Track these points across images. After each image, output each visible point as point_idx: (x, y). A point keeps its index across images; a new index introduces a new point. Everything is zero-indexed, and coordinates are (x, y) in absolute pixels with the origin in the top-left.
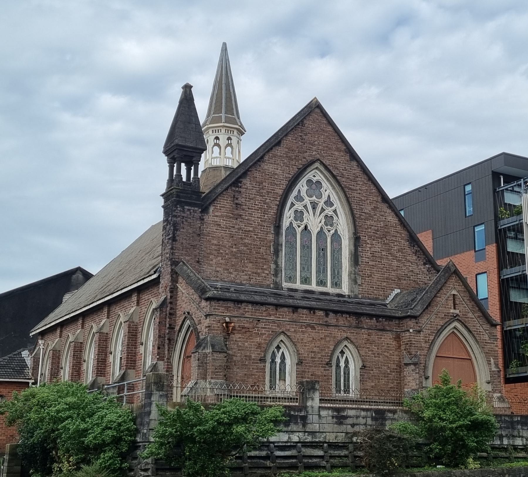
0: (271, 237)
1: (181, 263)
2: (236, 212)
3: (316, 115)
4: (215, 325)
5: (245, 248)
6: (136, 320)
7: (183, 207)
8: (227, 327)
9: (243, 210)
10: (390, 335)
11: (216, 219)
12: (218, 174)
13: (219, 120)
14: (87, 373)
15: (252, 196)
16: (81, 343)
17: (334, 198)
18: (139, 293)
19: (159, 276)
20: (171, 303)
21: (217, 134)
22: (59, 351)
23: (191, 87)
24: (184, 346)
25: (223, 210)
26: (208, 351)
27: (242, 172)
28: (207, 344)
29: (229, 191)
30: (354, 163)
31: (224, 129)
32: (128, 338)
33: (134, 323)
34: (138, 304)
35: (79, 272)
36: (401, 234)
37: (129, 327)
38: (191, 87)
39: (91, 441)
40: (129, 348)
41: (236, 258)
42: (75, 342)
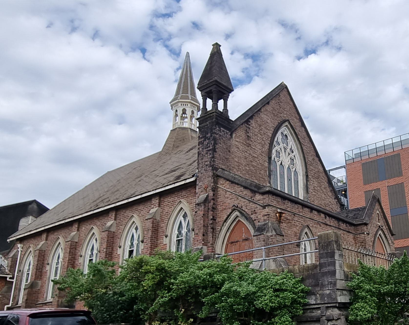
0: (266, 164)
1: (220, 170)
2: (248, 142)
3: (285, 92)
4: (272, 214)
5: (253, 169)
6: (158, 218)
7: (220, 128)
8: (280, 216)
9: (252, 141)
10: (351, 236)
11: (237, 143)
12: (186, 132)
13: (187, 98)
14: (84, 265)
15: (256, 133)
16: (76, 242)
17: (294, 148)
18: (160, 197)
19: (196, 179)
20: (213, 199)
21: (184, 107)
22: (45, 251)
23: (220, 46)
24: (228, 234)
25: (241, 138)
26: (270, 234)
27: (251, 115)
28: (268, 228)
29: (244, 125)
30: (303, 129)
31: (190, 104)
32: (152, 231)
33: (156, 220)
34: (46, 240)
35: (34, 203)
36: (325, 178)
37: (153, 223)
38: (220, 46)
39: (266, 304)
40: (152, 239)
41: (248, 175)
42: (40, 250)
